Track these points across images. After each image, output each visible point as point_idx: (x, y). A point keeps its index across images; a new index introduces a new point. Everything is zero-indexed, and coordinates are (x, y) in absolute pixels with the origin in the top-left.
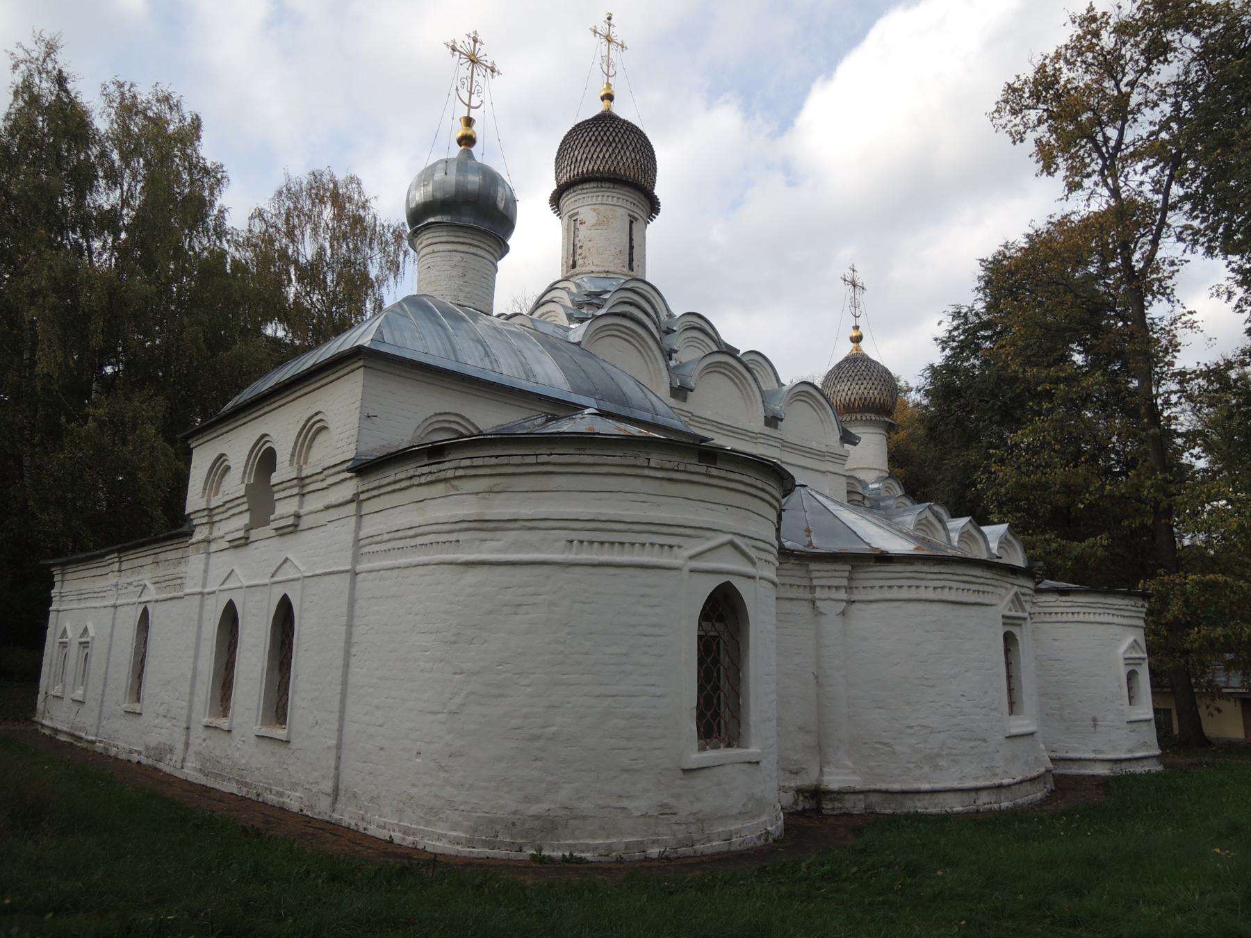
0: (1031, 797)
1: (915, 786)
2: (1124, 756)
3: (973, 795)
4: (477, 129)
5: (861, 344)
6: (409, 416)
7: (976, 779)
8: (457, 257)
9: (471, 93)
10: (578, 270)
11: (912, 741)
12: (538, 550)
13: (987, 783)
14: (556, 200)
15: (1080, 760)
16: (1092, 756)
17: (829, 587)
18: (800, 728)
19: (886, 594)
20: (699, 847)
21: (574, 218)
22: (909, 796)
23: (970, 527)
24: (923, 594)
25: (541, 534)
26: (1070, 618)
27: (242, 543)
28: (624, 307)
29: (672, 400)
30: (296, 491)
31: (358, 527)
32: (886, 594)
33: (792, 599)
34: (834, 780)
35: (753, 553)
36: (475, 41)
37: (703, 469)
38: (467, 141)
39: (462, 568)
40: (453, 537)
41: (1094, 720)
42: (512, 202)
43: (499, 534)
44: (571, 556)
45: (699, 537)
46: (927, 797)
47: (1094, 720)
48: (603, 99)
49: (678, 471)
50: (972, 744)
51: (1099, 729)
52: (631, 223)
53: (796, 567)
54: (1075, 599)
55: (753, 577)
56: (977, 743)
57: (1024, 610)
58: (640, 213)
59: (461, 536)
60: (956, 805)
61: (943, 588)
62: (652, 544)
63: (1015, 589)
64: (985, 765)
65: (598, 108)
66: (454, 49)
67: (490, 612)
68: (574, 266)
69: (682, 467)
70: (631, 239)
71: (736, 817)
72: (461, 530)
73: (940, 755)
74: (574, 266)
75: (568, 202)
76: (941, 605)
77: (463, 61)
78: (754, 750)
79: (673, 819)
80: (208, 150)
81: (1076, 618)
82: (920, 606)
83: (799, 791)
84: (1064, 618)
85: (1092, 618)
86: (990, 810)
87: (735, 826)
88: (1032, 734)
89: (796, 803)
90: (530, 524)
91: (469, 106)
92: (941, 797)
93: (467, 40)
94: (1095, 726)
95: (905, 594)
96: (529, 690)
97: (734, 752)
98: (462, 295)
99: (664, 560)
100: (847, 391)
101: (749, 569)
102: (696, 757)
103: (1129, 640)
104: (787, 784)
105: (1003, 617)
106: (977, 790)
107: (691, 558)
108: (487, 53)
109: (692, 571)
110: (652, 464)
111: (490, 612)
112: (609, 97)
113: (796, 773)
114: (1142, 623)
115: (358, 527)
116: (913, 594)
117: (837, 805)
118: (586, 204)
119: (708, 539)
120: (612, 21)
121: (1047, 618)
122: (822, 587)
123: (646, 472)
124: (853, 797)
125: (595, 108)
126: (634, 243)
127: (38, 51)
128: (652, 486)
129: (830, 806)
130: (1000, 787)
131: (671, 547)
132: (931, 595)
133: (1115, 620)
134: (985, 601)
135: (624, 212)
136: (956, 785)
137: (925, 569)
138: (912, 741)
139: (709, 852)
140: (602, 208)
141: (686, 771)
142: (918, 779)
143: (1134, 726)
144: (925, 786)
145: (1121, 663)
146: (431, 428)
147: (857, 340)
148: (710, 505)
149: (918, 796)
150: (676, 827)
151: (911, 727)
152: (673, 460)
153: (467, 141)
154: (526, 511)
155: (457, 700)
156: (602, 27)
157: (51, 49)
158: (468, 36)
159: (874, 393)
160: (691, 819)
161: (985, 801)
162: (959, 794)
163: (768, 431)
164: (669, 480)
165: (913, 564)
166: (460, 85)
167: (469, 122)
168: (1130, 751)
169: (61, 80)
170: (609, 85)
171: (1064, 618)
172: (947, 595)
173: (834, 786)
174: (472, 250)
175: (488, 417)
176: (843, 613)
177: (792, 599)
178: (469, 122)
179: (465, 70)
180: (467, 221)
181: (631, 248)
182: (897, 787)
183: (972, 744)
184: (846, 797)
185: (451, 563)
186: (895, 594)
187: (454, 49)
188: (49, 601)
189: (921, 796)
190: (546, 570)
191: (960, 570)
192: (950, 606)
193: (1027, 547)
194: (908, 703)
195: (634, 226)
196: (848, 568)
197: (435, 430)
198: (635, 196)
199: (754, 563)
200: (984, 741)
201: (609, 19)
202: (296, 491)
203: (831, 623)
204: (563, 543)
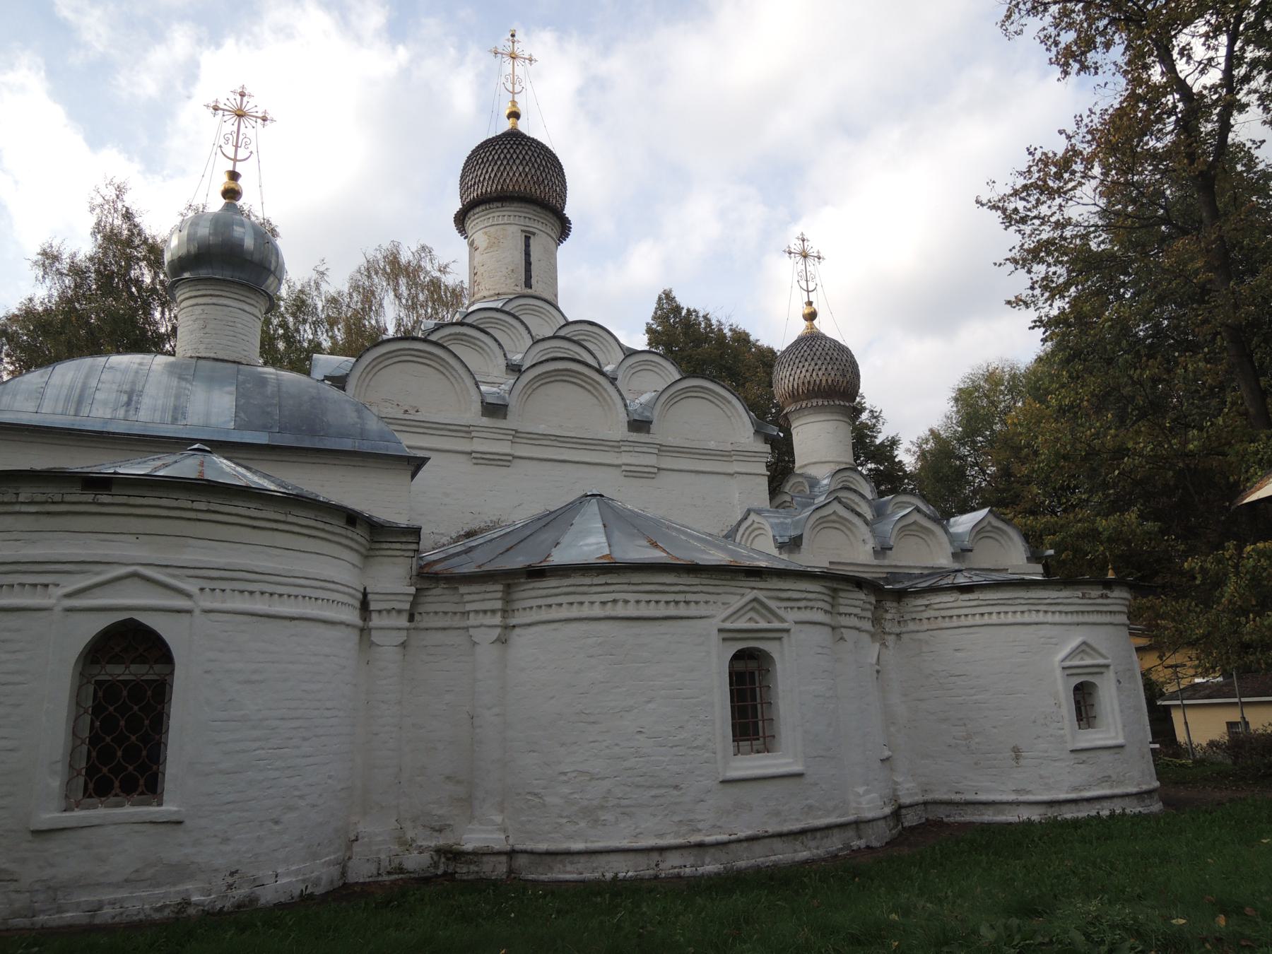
0: (773, 858)
1: (564, 846)
2: (1063, 796)
3: (655, 857)
5: (815, 322)
7: (661, 836)
8: (198, 310)
9: (237, 147)
11: (566, 790)
13: (680, 841)
15: (993, 803)
16: (1012, 797)
17: (485, 612)
18: (448, 778)
19: (545, 615)
20: (42, 919)
22: (559, 858)
24: (586, 611)
26: (978, 620)
29: (484, 419)
32: (545, 615)
33: (444, 629)
34: (472, 839)
35: (191, 586)
36: (242, 95)
37: (90, 498)
38: (231, 194)
41: (1017, 752)
45: (82, 572)
46: (583, 859)
47: (1017, 752)
49: (53, 503)
50: (653, 792)
51: (1022, 762)
52: (527, 239)
53: (446, 592)
54: (982, 596)
55: (189, 612)
56: (663, 791)
57: (782, 620)
58: (543, 230)
60: (624, 868)
61: (615, 601)
62: (23, 585)
63: (755, 593)
64: (676, 818)
65: (506, 125)
66: (216, 109)
69: (58, 498)
71: (118, 886)
73: (602, 807)
75: (476, 224)
76: (611, 623)
77: (226, 118)
78: (169, 808)
79: (12, 886)
81: (986, 619)
82: (583, 627)
83: (439, 851)
84: (963, 622)
85: (1010, 618)
86: (679, 876)
87: (107, 896)
88: (800, 775)
89: (436, 865)
91: (235, 160)
92: (603, 859)
93: (232, 97)
94: (1017, 758)
95: (564, 613)
97: (151, 811)
98: (202, 347)
104: (425, 843)
105: (720, 630)
106: (662, 850)
110: (21, 499)
113: (440, 831)
114: (1123, 619)
116: (575, 612)
117: (473, 868)
118: (480, 225)
119: (98, 574)
121: (947, 623)
122: (477, 612)
123: (17, 508)
124: (493, 859)
127: (111, 193)
128: (28, 522)
129: (465, 870)
130: (701, 845)
131: (46, 586)
132: (597, 611)
133: (1049, 618)
134: (703, 613)
136: (625, 844)
137: (587, 581)
138: (566, 790)
139: (54, 924)
140: (492, 229)
141: (37, 833)
142: (570, 837)
143: (1083, 756)
144: (578, 846)
145: (1058, 673)
147: (811, 316)
148: (102, 536)
149: (571, 858)
150: (14, 896)
151: (565, 774)
152: (53, 492)
153: (231, 194)
157: (120, 191)
158: (234, 92)
159: (821, 376)
160: (37, 887)
161: (671, 864)
162: (631, 856)
163: (634, 436)
164: (48, 513)
165: (568, 576)
166: (222, 142)
167: (234, 176)
168: (1075, 789)
169: (128, 216)
170: (514, 103)
171: (970, 621)
172: (620, 611)
173: (469, 847)
174: (214, 300)
176: (404, 645)
177: (444, 629)
178: (234, 176)
179: (230, 125)
180: (227, 274)
181: (528, 264)
182: (543, 847)
183: (653, 792)
184: (485, 859)
186: (554, 614)
187: (216, 109)
189: (576, 858)
191: (636, 578)
192: (625, 623)
193: (1033, 540)
194: (563, 745)
195: (532, 241)
196: (500, 587)
199: (189, 596)
200: (676, 787)
201: (513, 36)
203: (487, 653)
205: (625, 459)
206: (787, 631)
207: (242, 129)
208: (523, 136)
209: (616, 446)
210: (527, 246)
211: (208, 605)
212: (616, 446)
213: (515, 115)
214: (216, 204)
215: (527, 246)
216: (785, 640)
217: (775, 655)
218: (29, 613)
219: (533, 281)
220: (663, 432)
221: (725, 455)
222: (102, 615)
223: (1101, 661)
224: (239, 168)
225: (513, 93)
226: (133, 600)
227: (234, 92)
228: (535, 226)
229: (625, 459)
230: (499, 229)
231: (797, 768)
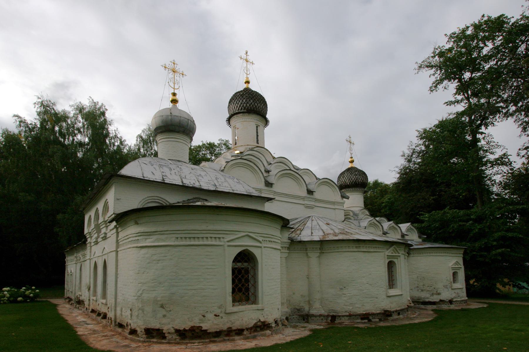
4: (177, 97)
6: (134, 200)
9: (174, 84)
10: (236, 146)
12: (164, 241)
14: (229, 120)
21: (235, 127)
23: (393, 225)
25: (166, 236)
27: (96, 243)
28: (252, 158)
30: (104, 226)
31: (117, 236)
35: (260, 239)
36: (174, 64)
38: (174, 101)
39: (139, 249)
40: (137, 238)
42: (427, 136)
43: (151, 237)
44: (177, 243)
48: (245, 83)
52: (257, 127)
55: (261, 247)
57: (399, 253)
58: (261, 124)
59: (139, 238)
62: (211, 238)
65: (245, 86)
67: (149, 263)
68: (236, 144)
70: (257, 132)
72: (139, 236)
74: (236, 144)
75: (232, 121)
80: (108, 115)
88: (402, 295)
90: (161, 233)
91: (174, 89)
93: (170, 63)
96: (163, 288)
99: (218, 243)
100: (346, 180)
101: (258, 244)
102: (230, 308)
103: (454, 261)
105: (387, 256)
107: (228, 241)
108: (180, 68)
109: (229, 246)
111: (149, 263)
112: (248, 82)
115: (117, 236)
118: (237, 121)
119: (236, 235)
120: (248, 54)
125: (241, 87)
126: (259, 134)
131: (219, 238)
135: (254, 123)
146: (147, 202)
153: (174, 101)
154: (160, 229)
155: (140, 292)
156: (244, 56)
158: (171, 62)
163: (308, 196)
167: (174, 94)
170: (247, 78)
175: (173, 199)
178: (174, 94)
181: (257, 136)
185: (136, 247)
188: (65, 263)
190: (168, 248)
195: (258, 128)
197: (148, 203)
198: (258, 117)
199: (260, 242)
200: (377, 298)
202: (104, 226)
204: (174, 239)
205: (306, 202)
206: (399, 256)
207: (176, 77)
208: (250, 90)
209: (303, 198)
210: (257, 130)
211: (266, 245)
212: (303, 198)
213: (248, 82)
214: (168, 105)
215: (257, 130)
216: (399, 259)
217: (396, 263)
218: (215, 247)
219: (259, 142)
220: (316, 195)
221: (333, 203)
222: (237, 248)
223: (460, 266)
224: (176, 92)
225: (247, 74)
226: (247, 243)
227: (171, 62)
228: (260, 123)
229: (306, 202)
230: (247, 123)
231: (400, 293)
